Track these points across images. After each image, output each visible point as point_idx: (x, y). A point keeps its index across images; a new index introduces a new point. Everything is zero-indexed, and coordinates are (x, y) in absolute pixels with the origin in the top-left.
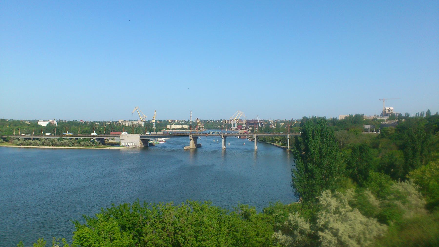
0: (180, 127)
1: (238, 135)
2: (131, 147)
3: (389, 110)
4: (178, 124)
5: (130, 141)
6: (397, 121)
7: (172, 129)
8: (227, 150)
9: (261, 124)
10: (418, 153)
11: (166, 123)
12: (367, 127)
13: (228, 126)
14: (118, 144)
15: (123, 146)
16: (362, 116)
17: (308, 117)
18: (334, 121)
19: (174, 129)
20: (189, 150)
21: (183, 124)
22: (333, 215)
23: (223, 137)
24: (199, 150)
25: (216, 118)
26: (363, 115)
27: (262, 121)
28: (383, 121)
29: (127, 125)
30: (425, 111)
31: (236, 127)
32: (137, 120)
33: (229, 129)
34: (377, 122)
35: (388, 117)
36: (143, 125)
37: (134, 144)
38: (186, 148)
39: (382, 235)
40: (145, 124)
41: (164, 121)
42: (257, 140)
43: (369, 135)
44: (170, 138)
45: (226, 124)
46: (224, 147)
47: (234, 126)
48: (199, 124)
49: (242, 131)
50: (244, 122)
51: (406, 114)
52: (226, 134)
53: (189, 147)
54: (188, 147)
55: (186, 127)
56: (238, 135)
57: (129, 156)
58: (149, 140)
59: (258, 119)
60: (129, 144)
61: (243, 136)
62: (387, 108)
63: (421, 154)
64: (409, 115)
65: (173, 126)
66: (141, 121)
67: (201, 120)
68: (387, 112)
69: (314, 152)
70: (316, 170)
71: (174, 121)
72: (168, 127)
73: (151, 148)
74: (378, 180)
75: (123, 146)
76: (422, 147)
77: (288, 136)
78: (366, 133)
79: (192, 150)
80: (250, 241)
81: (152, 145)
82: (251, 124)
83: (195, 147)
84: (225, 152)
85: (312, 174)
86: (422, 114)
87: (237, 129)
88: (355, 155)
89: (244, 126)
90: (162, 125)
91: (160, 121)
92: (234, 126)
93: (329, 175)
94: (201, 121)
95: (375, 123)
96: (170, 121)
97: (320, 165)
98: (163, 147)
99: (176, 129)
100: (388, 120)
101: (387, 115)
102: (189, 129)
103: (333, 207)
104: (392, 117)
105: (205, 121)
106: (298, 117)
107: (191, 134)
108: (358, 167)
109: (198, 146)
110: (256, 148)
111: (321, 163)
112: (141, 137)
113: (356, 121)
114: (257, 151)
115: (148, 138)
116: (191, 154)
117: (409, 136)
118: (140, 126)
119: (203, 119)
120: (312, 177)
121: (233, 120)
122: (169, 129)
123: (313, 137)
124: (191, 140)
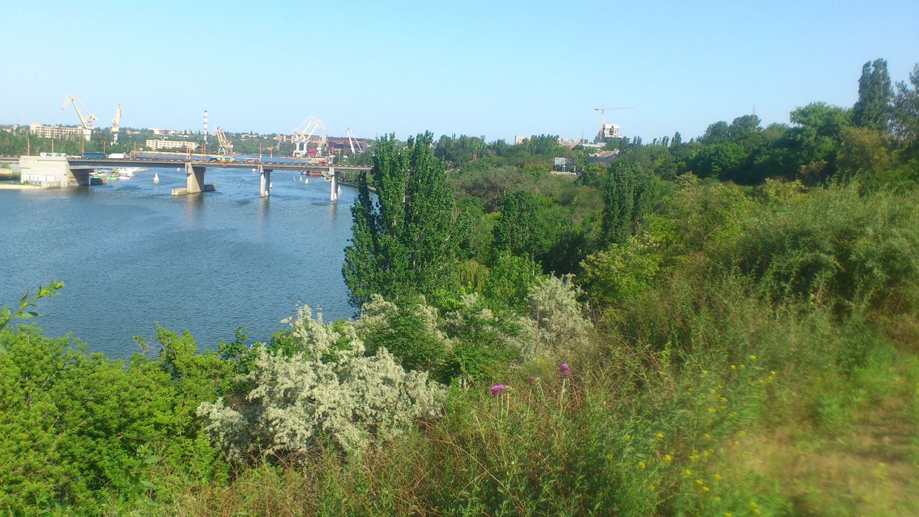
0: (178, 145)
1: (304, 169)
2: (45, 185)
4: (175, 138)
5: (47, 172)
6: (617, 152)
7: (160, 150)
8: (272, 199)
9: (356, 146)
10: (628, 217)
11: (148, 135)
12: (559, 161)
13: (288, 148)
14: (16, 178)
15: (27, 183)
16: (554, 139)
17: (450, 135)
18: (499, 148)
19: (164, 149)
20: (184, 195)
21: (188, 140)
22: (320, 363)
23: (262, 171)
24: (208, 198)
25: (264, 130)
26: (558, 137)
27: (358, 140)
28: (593, 150)
29: (48, 136)
30: (671, 136)
31: (305, 151)
32: (75, 126)
33: (290, 154)
34: (581, 152)
35: (603, 144)
36: (88, 138)
37: (53, 180)
38: (176, 192)
39: (432, 413)
40: (93, 136)
41: (143, 131)
42: (336, 180)
43: (559, 179)
44: (147, 169)
45: (283, 144)
46: (263, 192)
47: (301, 148)
48: (221, 140)
49: (317, 160)
50: (324, 141)
51: (635, 138)
52: (270, 165)
53: (184, 189)
54: (183, 190)
55: (193, 146)
56: (304, 169)
58: (92, 171)
59: (349, 135)
60: (42, 179)
61: (312, 171)
62: (608, 126)
63: (633, 219)
64: (640, 141)
65: (162, 144)
66: (84, 127)
67: (227, 134)
69: (392, 208)
70: (396, 247)
71: (166, 132)
72: (150, 143)
73: (97, 189)
74: (515, 273)
75: (27, 183)
76: (635, 205)
78: (559, 173)
79: (190, 197)
80: (135, 425)
81: (98, 182)
82: (337, 145)
83: (199, 190)
84: (267, 204)
85: (387, 256)
86: (665, 139)
87: (306, 156)
88: (509, 216)
89: (319, 149)
90: (131, 140)
91: (133, 130)
92: (301, 148)
93: (423, 261)
94: (228, 135)
95: (579, 155)
96: (157, 132)
97: (405, 239)
98: (128, 188)
99: (169, 150)
100: (603, 149)
101: (605, 140)
102: (198, 150)
103: (323, 346)
105: (238, 135)
107: (189, 161)
108: (513, 242)
109: (208, 189)
110: (333, 197)
111: (407, 234)
112: (71, 163)
113: (542, 147)
114: (336, 203)
115: (88, 167)
116: (190, 208)
118: (80, 138)
119: (233, 130)
120: (386, 262)
121: (299, 136)
122: (150, 149)
123: (392, 175)
124: (188, 175)
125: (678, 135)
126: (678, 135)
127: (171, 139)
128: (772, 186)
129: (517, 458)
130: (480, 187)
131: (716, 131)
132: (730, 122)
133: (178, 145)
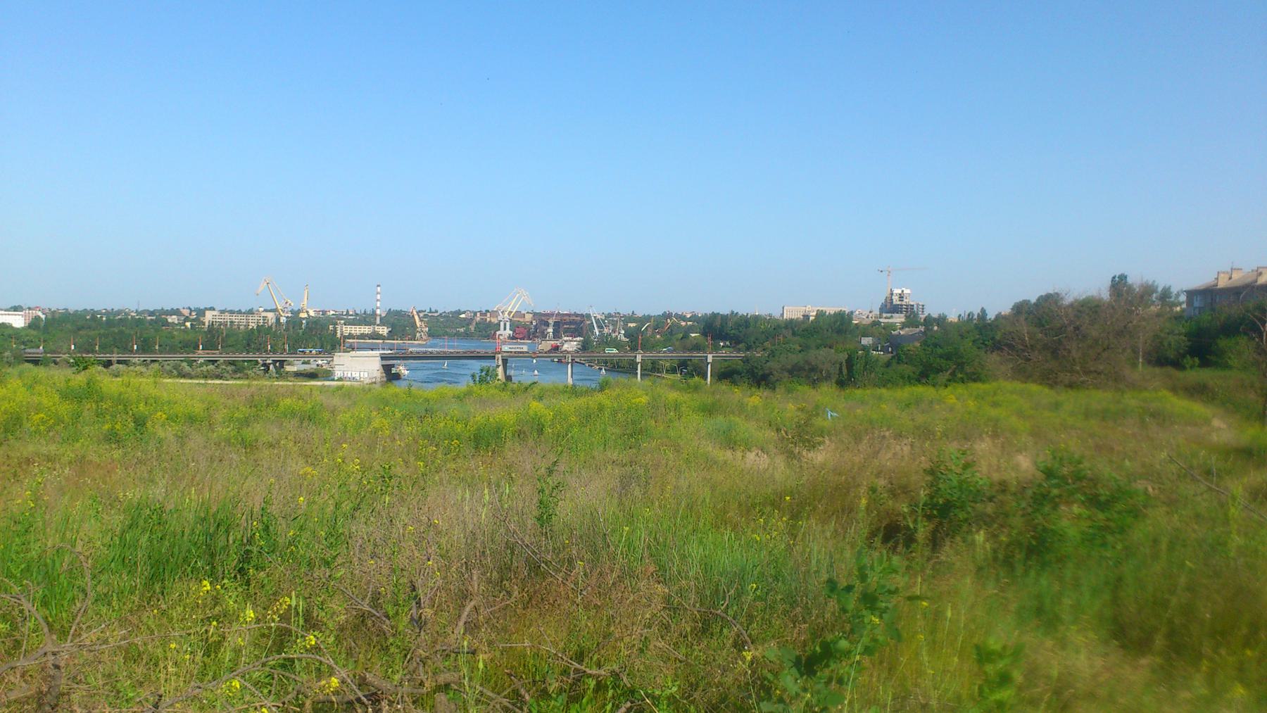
0: (366, 330)
3: (901, 297)
5: (358, 367)
6: (922, 328)
9: (600, 327)
13: (487, 329)
15: (340, 379)
57: (350, 394)
60: (356, 375)
68: (896, 300)
77: (639, 359)
100: (904, 326)
104: (912, 315)
106: (656, 311)
117: (1083, 382)
125: (983, 310)
126: (983, 310)
127: (353, 323)
128: (1107, 596)
129: (848, 547)
130: (801, 369)
131: (1020, 308)
132: (1033, 300)
133: (366, 330)
